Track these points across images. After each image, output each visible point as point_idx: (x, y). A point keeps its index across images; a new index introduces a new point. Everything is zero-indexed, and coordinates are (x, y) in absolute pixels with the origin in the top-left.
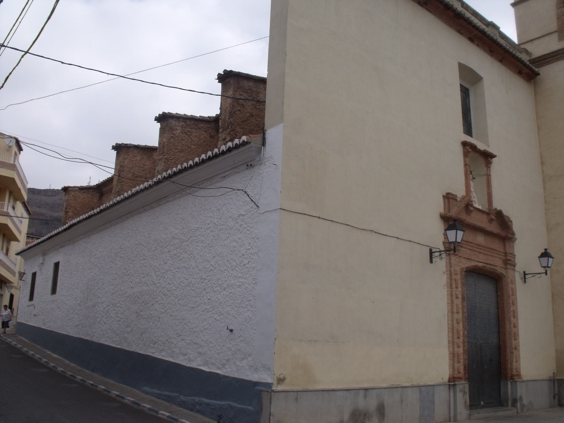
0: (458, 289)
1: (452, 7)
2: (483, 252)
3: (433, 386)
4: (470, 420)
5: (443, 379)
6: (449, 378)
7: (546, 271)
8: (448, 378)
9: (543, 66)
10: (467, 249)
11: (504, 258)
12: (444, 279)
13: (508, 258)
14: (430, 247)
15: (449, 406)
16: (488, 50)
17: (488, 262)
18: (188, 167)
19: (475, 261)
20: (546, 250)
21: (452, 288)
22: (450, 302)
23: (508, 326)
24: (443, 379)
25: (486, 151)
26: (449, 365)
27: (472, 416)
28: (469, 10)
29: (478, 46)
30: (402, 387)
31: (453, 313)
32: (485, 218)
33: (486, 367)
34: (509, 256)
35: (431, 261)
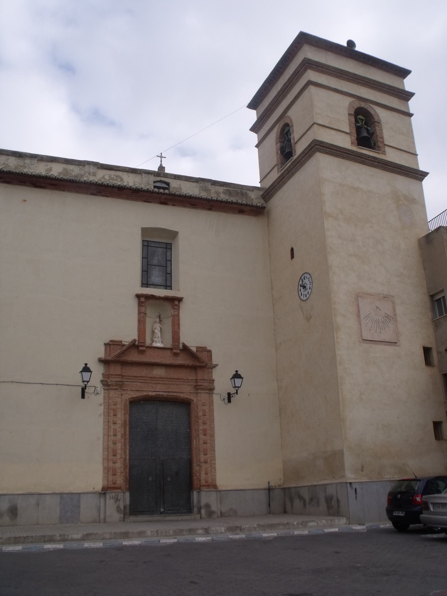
0: (118, 416)
1: (279, 141)
2: (150, 382)
3: (80, 494)
4: (124, 521)
5: (94, 488)
6: (102, 488)
7: (237, 391)
8: (102, 487)
9: (271, 198)
10: (137, 382)
11: (195, 384)
12: (101, 409)
13: (199, 384)
14: (81, 386)
15: (99, 510)
16: (189, 205)
17: (170, 390)
18: (175, 321)
19: (148, 391)
20: (237, 371)
21: (109, 416)
22: (107, 427)
23: (195, 443)
24: (94, 488)
25: (166, 297)
26: (103, 478)
27: (127, 519)
28: (169, 176)
29: (174, 205)
30: (40, 494)
31: (109, 436)
32: (168, 353)
33: (169, 480)
34: (199, 382)
35: (83, 396)
